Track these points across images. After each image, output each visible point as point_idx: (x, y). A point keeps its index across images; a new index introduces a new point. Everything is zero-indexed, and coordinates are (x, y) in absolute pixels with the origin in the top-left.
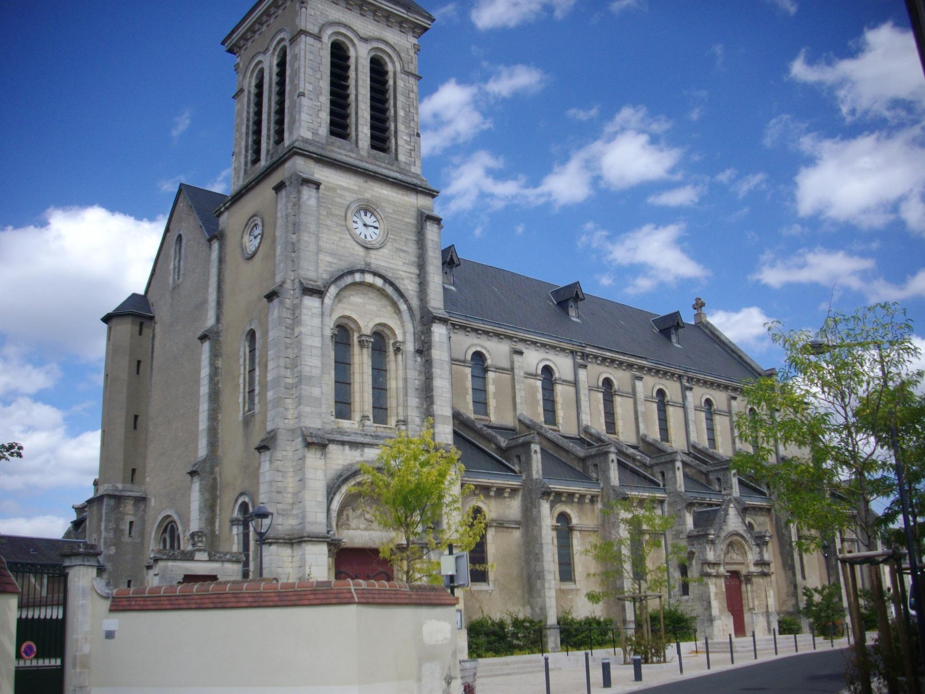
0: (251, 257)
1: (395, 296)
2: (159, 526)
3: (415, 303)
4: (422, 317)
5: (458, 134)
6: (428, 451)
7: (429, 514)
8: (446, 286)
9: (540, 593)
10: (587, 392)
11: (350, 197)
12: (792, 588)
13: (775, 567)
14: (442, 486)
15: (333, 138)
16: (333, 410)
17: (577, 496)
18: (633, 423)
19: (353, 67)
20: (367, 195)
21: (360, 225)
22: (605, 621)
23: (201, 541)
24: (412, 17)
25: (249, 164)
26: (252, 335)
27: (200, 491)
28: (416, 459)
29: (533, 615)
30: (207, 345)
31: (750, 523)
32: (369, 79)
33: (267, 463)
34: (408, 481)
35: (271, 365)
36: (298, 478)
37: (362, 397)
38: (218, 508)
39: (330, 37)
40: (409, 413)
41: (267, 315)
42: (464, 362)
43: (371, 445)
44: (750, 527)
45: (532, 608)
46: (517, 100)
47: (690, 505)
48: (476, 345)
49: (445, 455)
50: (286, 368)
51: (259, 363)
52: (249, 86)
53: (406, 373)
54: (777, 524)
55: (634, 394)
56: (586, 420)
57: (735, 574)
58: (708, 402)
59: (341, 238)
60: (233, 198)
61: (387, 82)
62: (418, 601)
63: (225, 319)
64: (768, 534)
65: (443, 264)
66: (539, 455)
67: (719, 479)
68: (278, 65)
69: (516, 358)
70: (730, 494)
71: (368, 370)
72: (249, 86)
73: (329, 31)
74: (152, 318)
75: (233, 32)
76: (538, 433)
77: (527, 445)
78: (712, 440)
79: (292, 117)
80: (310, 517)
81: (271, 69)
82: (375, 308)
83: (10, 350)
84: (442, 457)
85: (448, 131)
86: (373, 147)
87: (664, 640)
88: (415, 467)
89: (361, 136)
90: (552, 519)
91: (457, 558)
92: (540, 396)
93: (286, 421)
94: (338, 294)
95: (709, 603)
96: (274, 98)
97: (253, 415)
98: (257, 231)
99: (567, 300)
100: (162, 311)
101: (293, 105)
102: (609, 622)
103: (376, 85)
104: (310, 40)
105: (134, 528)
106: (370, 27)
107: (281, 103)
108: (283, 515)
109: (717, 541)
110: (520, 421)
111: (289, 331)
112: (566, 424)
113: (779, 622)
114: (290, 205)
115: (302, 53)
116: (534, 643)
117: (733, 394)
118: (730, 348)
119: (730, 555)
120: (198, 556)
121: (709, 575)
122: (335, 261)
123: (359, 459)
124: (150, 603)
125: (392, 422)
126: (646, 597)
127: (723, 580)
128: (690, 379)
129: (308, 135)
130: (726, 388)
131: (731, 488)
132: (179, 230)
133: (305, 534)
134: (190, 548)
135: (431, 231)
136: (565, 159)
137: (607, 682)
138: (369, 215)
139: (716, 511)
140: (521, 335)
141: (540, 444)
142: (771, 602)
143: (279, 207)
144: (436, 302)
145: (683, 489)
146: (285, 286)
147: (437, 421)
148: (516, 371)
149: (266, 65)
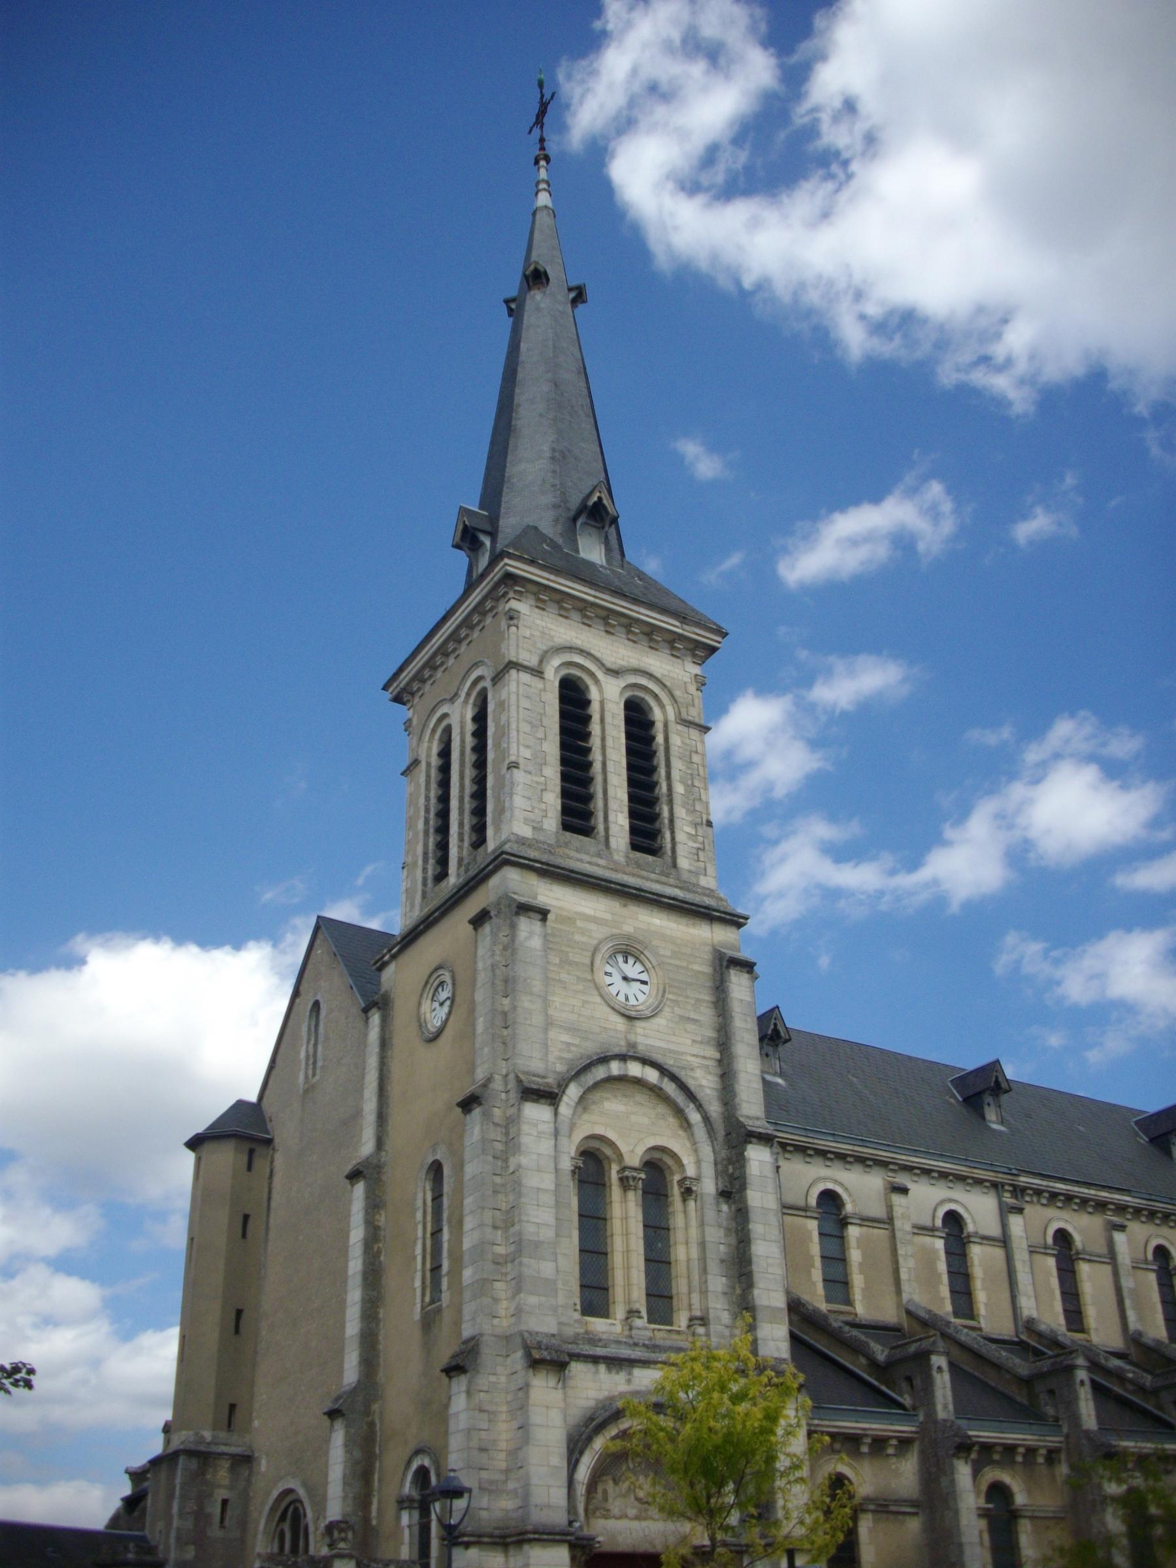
1: (680, 1099)
2: (273, 1509)
3: (715, 1109)
4: (728, 1134)
5: (769, 787)
6: (743, 1372)
7: (751, 1489)
8: (769, 1077)
10: (1026, 1256)
14: (773, 1439)
15: (568, 834)
16: (578, 1302)
17: (1021, 1450)
19: (596, 718)
20: (628, 929)
23: (344, 1540)
24: (691, 632)
25: (430, 882)
26: (436, 1169)
27: (346, 1445)
28: (723, 1389)
30: (360, 1188)
32: (623, 735)
33: (463, 1396)
34: (710, 1429)
35: (469, 1223)
36: (515, 1424)
37: (627, 1276)
38: (376, 1476)
39: (557, 669)
40: (711, 1305)
41: (461, 1137)
42: (805, 1209)
43: (645, 1363)
46: (866, 713)
48: (825, 1179)
49: (775, 1380)
50: (495, 1227)
52: (429, 756)
55: (1112, 1256)
56: (1028, 1306)
59: (585, 1002)
60: (403, 939)
61: (653, 738)
63: (389, 1145)
65: (761, 1039)
66: (946, 1376)
68: (474, 719)
69: (897, 1199)
72: (429, 756)
73: (556, 662)
74: (269, 1142)
75: (401, 669)
76: (944, 1335)
77: (923, 1357)
79: (498, 800)
80: (539, 1495)
81: (462, 727)
82: (645, 1121)
83: (17, 1176)
84: (769, 1384)
85: (753, 780)
86: (635, 847)
88: (721, 1404)
89: (614, 829)
90: (978, 1495)
92: (942, 1266)
93: (496, 1321)
94: (582, 1099)
96: (469, 773)
97: (439, 1310)
98: (444, 995)
99: (979, 1094)
100: (286, 1131)
101: (500, 784)
103: (635, 730)
104: (525, 677)
105: (229, 1513)
107: (480, 780)
108: (490, 1492)
110: (909, 1313)
112: (992, 1316)
114: (498, 949)
115: (513, 698)
122: (577, 1041)
123: (623, 1388)
129: (526, 832)
132: (316, 994)
133: (530, 1528)
134: (325, 1551)
135: (738, 983)
136: (963, 813)
138: (631, 960)
140: (904, 1158)
141: (947, 1354)
143: (480, 952)
144: (751, 1106)
146: (491, 1086)
147: (759, 1316)
148: (898, 1223)
149: (454, 721)
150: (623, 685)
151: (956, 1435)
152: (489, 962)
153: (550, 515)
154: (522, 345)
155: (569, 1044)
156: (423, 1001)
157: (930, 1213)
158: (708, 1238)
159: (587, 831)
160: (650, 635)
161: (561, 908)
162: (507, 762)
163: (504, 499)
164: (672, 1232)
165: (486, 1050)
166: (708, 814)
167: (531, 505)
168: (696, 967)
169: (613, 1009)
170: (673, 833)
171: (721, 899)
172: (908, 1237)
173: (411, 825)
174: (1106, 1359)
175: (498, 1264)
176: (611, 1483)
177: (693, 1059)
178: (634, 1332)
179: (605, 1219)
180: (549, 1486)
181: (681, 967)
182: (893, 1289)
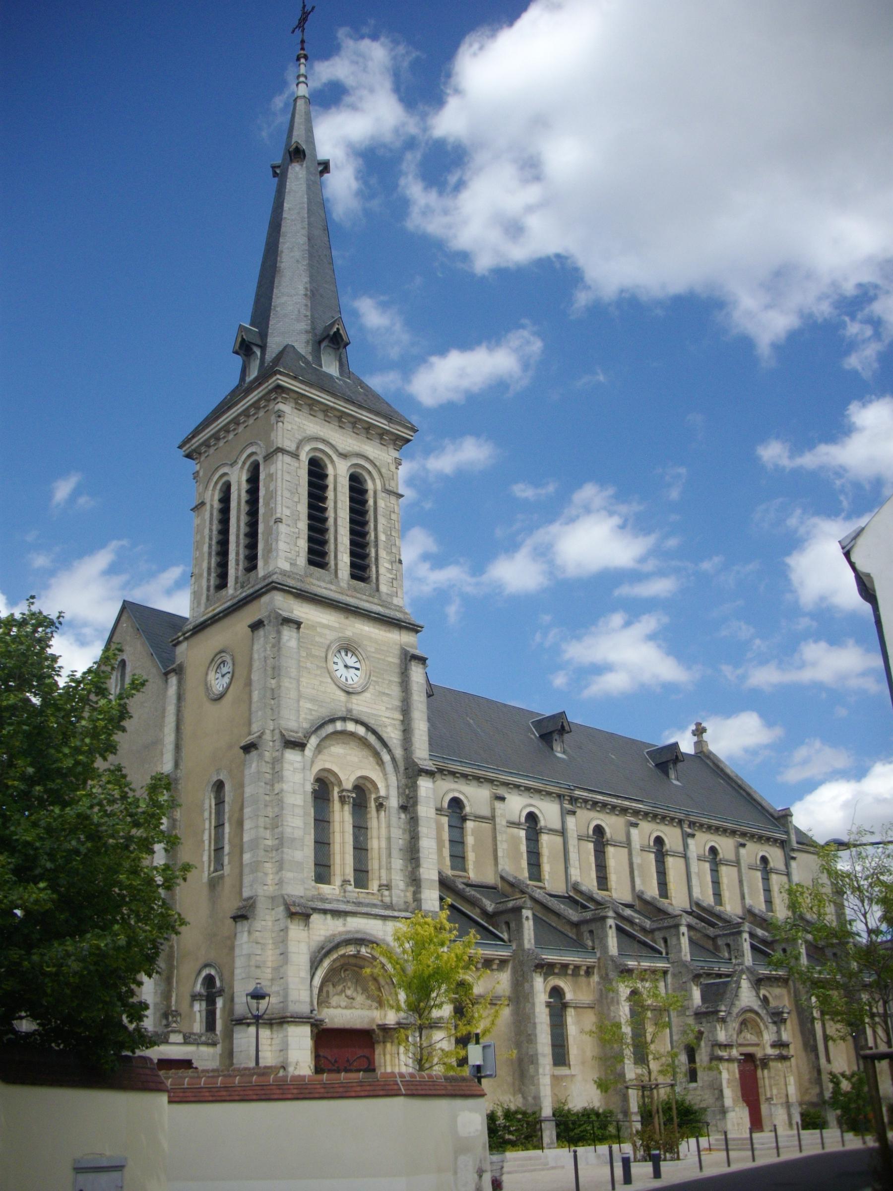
0: (220, 697)
3: (398, 752)
4: (406, 769)
9: (534, 1080)
11: (331, 636)
12: (816, 1074)
13: (795, 1049)
15: (312, 567)
17: (571, 967)
18: (628, 877)
20: (349, 633)
21: (341, 666)
22: (604, 1112)
23: (175, 1022)
26: (219, 786)
29: (524, 1105)
31: (765, 996)
33: (246, 934)
35: (247, 825)
36: (278, 952)
37: (343, 859)
39: (308, 453)
40: (393, 877)
44: (765, 1001)
45: (524, 1098)
47: (697, 977)
48: (453, 790)
50: (266, 828)
51: (230, 819)
52: (212, 500)
53: (389, 831)
54: (795, 996)
55: (628, 844)
56: (575, 874)
57: (749, 1058)
58: (713, 850)
60: (194, 628)
61: (366, 501)
62: (453, 1093)
64: (786, 1010)
66: (531, 922)
67: (728, 945)
69: (498, 804)
70: (742, 964)
71: (349, 829)
72: (212, 500)
73: (307, 448)
77: (517, 910)
78: (718, 895)
80: (293, 995)
81: (239, 485)
82: (356, 759)
86: (353, 576)
87: (678, 1135)
89: (341, 565)
91: (484, 1047)
92: (523, 848)
93: (266, 888)
94: (318, 745)
95: (721, 1091)
96: (244, 519)
97: (222, 877)
98: (225, 670)
101: (269, 532)
102: (608, 1114)
104: (287, 459)
106: (350, 441)
109: (728, 1019)
110: (502, 878)
111: (268, 787)
112: (553, 880)
113: (802, 1115)
114: (268, 647)
115: (279, 473)
116: (528, 1137)
117: (741, 840)
118: (736, 783)
119: (743, 1034)
120: (173, 1038)
121: (720, 1059)
122: (316, 708)
124: (190, 1094)
125: (374, 886)
126: (657, 1085)
127: (736, 1065)
128: (692, 824)
130: (733, 833)
131: (743, 955)
133: (289, 1014)
135: (417, 674)
137: (628, 1179)
139: (726, 984)
141: (532, 909)
142: (792, 1090)
143: (256, 647)
144: (421, 752)
145: (688, 958)
146: (264, 737)
148: (498, 820)
150: (349, 464)
151: (536, 959)
152: (263, 655)
153: (304, 337)
154: (285, 205)
155: (311, 710)
156: (210, 672)
157: (518, 813)
158: (392, 835)
159: (323, 565)
160: (368, 430)
161: (308, 620)
162: (274, 517)
163: (271, 323)
164: (369, 831)
165: (260, 713)
166: (400, 555)
167: (290, 328)
168: (390, 659)
169: (339, 687)
170: (377, 567)
171: (406, 613)
172: (504, 829)
173: (198, 547)
174: (623, 910)
175: (267, 851)
176: (331, 986)
177: (386, 720)
178: (347, 894)
179: (329, 822)
180: (299, 990)
181: (379, 659)
182: (493, 862)
